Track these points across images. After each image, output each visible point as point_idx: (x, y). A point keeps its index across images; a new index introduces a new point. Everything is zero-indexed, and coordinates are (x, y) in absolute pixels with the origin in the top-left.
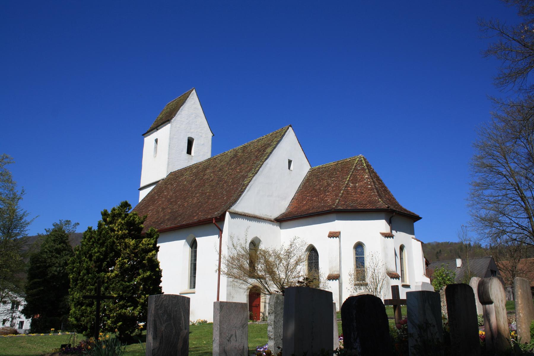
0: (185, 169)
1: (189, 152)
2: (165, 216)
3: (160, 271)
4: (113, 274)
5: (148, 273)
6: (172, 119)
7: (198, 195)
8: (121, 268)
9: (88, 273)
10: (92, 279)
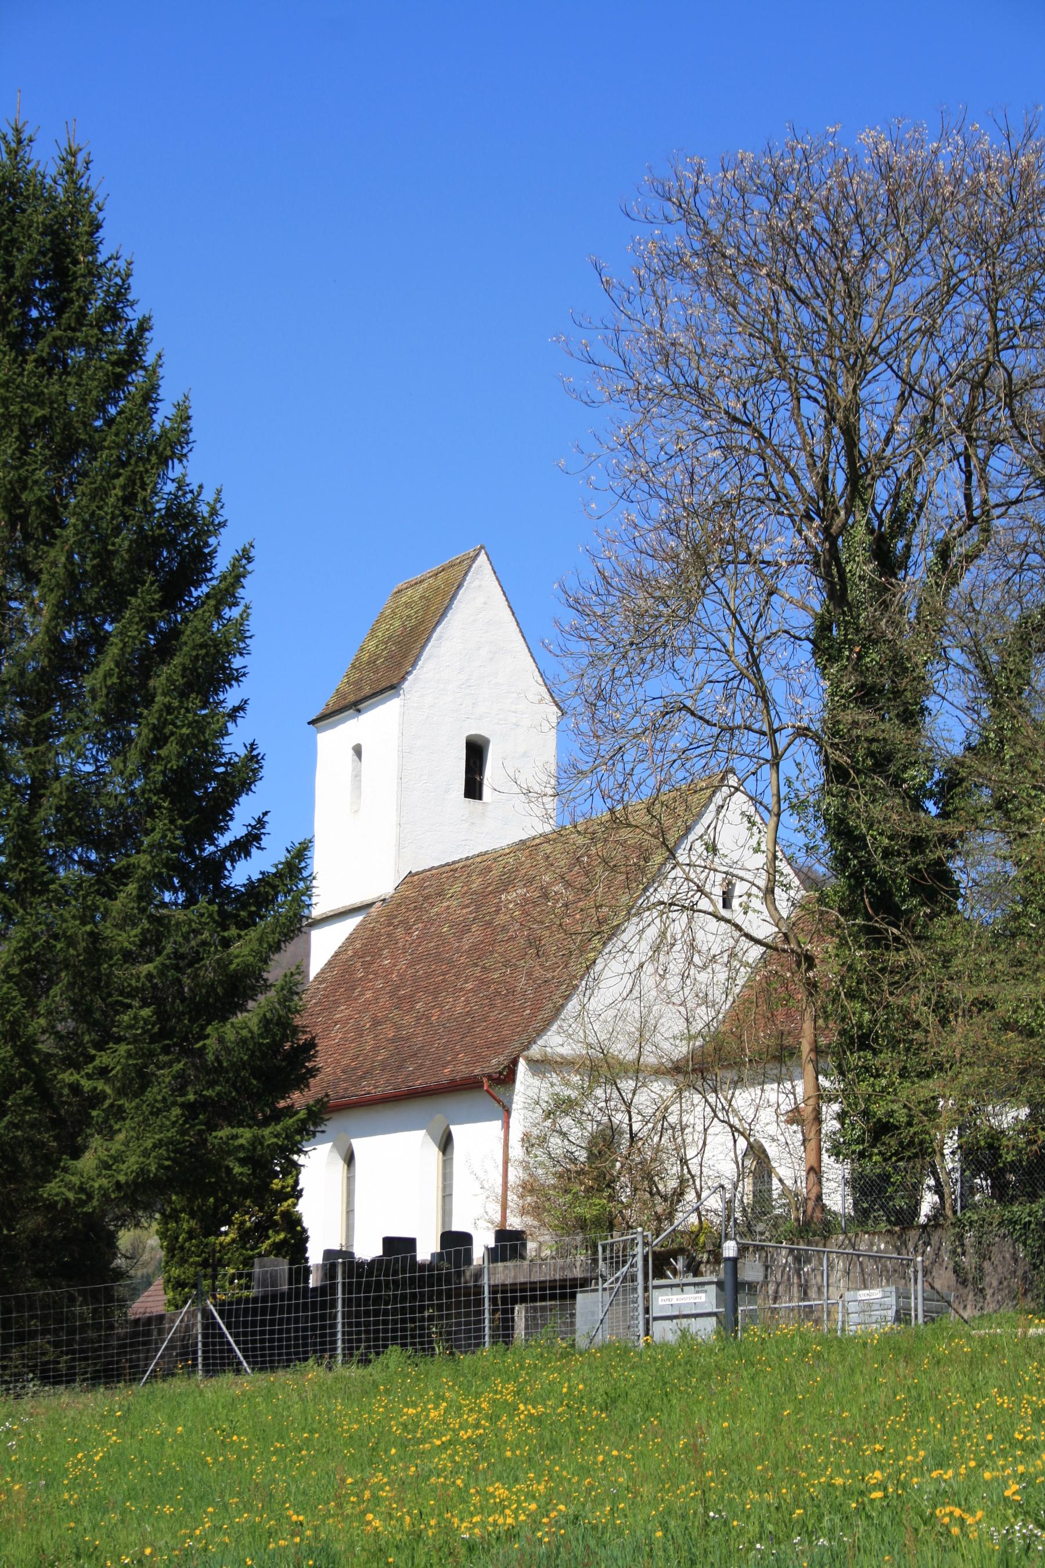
0: (452, 870)
1: (473, 789)
2: (376, 1049)
3: (304, 1230)
4: (228, 1239)
5: (282, 1236)
6: (403, 679)
7: (469, 986)
8: (239, 1229)
9: (190, 1238)
10: (198, 1246)
